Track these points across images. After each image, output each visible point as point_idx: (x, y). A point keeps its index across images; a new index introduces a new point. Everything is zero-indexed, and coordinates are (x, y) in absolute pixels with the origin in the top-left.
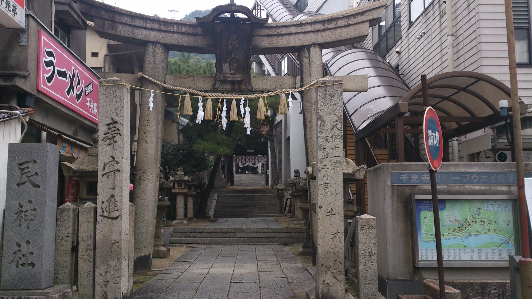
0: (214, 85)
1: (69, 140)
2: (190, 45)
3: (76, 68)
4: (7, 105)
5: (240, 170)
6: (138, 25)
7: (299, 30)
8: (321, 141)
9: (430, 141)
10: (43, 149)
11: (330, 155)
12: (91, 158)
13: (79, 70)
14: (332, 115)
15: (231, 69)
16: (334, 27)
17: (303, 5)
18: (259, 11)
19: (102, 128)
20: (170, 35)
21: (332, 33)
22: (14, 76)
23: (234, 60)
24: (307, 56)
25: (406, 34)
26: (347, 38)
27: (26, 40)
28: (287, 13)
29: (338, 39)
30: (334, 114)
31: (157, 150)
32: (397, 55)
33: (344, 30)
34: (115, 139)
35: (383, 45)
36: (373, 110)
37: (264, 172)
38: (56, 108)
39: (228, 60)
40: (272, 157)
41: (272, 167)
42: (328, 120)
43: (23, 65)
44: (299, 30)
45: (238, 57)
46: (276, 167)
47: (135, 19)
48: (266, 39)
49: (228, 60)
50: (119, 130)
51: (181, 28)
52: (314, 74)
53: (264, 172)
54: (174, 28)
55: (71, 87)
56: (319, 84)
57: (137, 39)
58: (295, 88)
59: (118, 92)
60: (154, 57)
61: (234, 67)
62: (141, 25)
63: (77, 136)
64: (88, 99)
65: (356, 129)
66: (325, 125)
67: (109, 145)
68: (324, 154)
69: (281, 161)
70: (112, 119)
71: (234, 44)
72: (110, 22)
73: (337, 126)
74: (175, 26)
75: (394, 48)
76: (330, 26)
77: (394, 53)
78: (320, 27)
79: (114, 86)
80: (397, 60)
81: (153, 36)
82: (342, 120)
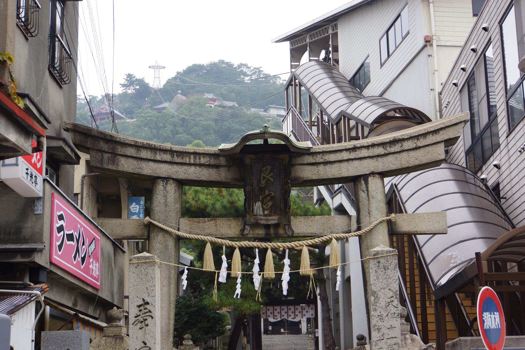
0: (243, 230)
1: (84, 318)
2: (211, 179)
3: (82, 226)
4: (21, 282)
5: (270, 328)
6: (144, 157)
7: (353, 155)
8: (375, 320)
9: (487, 325)
10: (77, 337)
11: (386, 336)
12: (109, 340)
13: (84, 227)
14: (387, 290)
15: (264, 210)
16: (398, 150)
17: (362, 78)
18: (298, 88)
19: (133, 310)
20: (186, 167)
21: (396, 158)
22: (33, 251)
23: (269, 198)
24: (365, 189)
25: (505, 142)
26: (417, 164)
27: (41, 208)
28: (341, 95)
29: (404, 166)
30: (389, 289)
31: (169, 319)
32: (496, 169)
33: (412, 153)
34: (146, 322)
35: (478, 149)
36: (456, 257)
37: (312, 331)
38: (63, 278)
39: (261, 197)
40: (323, 311)
41: (323, 325)
42: (382, 296)
43: (37, 237)
44: (353, 155)
45: (273, 194)
46: (330, 326)
47: (142, 150)
48: (310, 168)
49: (261, 197)
50: (150, 312)
51: (200, 159)
52: (374, 212)
53: (312, 331)
54: (190, 158)
55: (78, 250)
56: (370, 256)
57: (144, 175)
58: (349, 232)
59: (150, 270)
60: (165, 197)
61: (269, 206)
62: (149, 158)
63: (76, 306)
64: (91, 260)
65: (435, 285)
66: (379, 302)
67: (140, 329)
68: (379, 335)
69: (337, 315)
70: (143, 300)
71: (269, 177)
72: (110, 155)
73: (393, 303)
74: (192, 156)
75: (492, 159)
76: (393, 150)
77: (492, 166)
78: (380, 151)
79: (145, 263)
80: (497, 175)
81: (164, 170)
82: (398, 296)
